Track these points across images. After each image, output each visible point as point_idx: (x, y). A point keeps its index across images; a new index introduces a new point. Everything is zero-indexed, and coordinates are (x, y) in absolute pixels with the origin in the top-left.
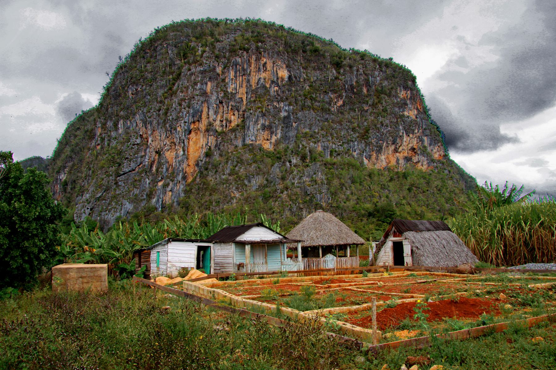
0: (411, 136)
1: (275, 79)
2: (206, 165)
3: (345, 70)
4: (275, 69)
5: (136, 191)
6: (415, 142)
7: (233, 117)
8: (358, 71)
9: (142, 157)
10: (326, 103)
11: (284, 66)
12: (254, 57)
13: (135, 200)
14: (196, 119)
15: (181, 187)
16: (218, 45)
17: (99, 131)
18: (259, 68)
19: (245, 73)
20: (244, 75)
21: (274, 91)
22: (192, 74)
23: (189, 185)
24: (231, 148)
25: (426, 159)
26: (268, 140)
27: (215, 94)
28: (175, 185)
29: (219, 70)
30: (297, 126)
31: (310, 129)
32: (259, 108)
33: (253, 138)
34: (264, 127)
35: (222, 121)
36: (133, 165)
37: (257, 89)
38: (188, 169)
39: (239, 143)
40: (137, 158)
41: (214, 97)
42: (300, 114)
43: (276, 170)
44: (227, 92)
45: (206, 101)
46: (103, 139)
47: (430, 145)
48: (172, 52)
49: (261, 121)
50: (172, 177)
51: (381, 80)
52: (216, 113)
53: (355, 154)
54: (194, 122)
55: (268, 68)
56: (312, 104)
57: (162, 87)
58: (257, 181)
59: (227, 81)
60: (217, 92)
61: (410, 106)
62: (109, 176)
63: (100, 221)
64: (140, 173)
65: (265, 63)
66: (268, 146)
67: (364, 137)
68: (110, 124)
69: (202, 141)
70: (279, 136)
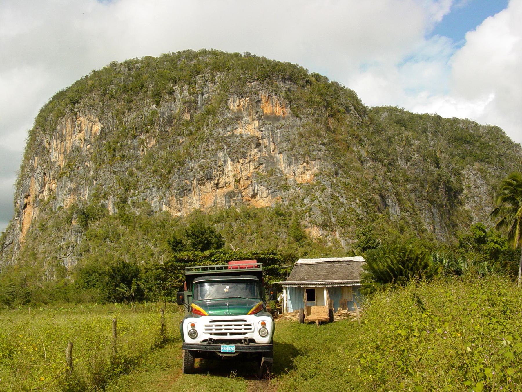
11: (97, 120)
47: (289, 165)
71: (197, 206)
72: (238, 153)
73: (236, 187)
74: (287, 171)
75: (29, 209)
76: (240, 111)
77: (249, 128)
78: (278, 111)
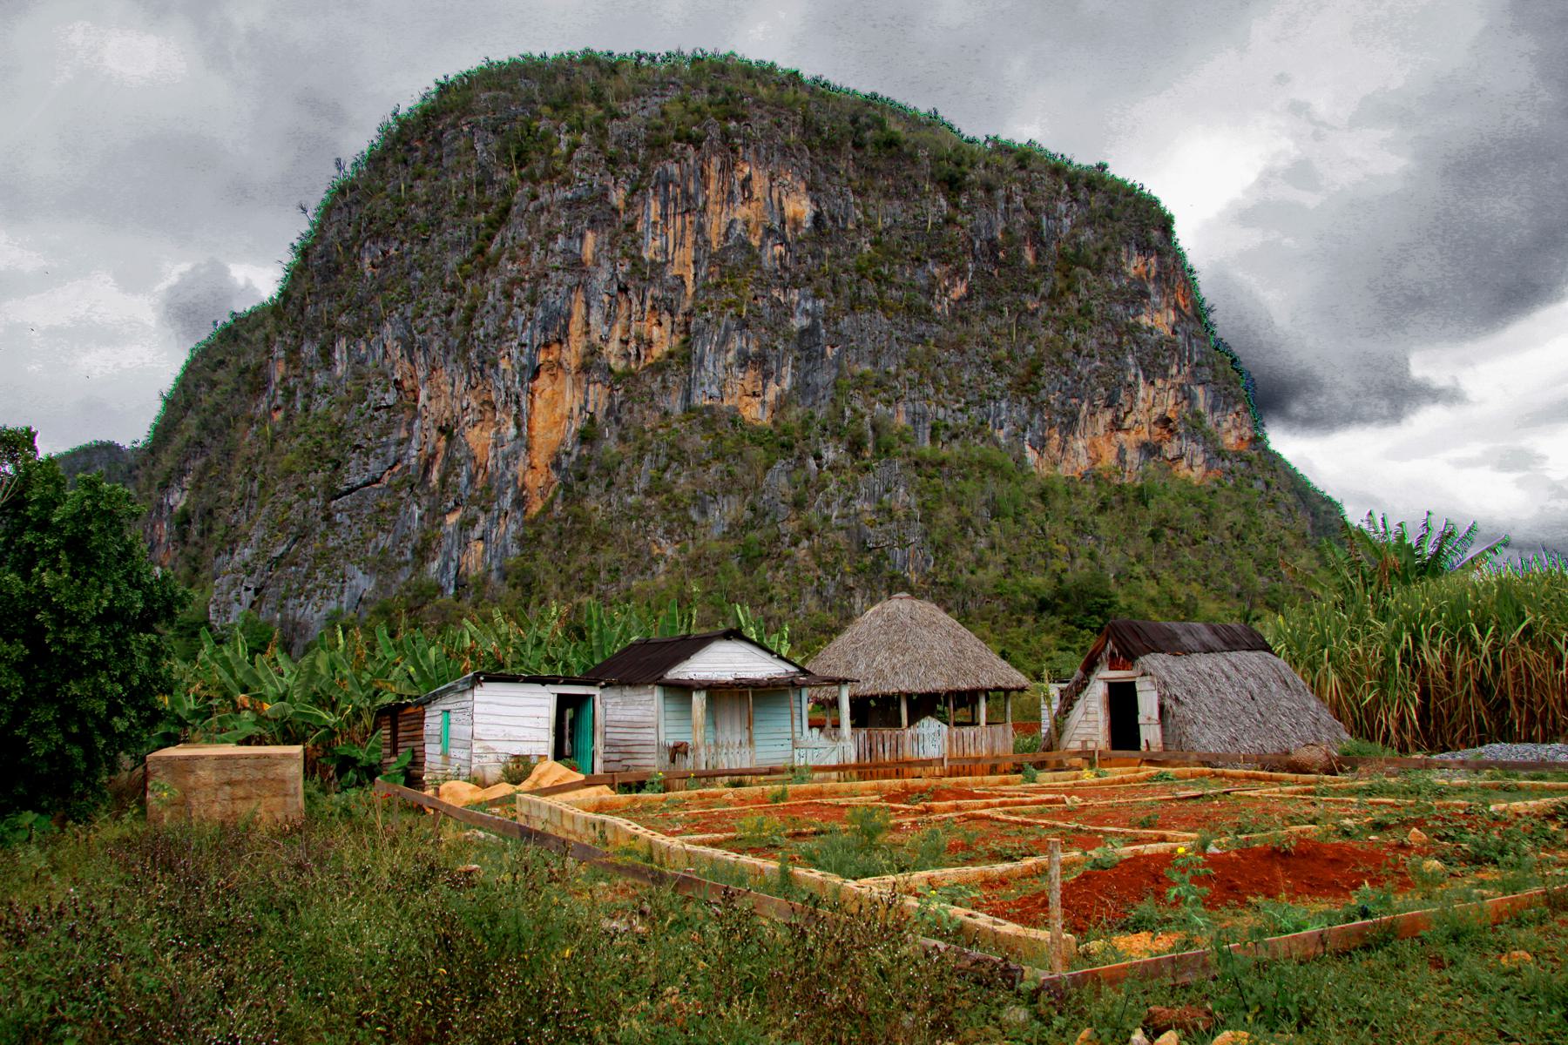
0: (1159, 383)
1: (777, 223)
2: (582, 467)
3: (972, 199)
4: (775, 195)
5: (385, 541)
6: (1171, 402)
7: (656, 331)
8: (1008, 199)
9: (400, 443)
10: (921, 290)
11: (802, 187)
12: (716, 161)
13: (382, 566)
14: (551, 335)
15: (509, 529)
16: (615, 127)
17: (278, 371)
18: (731, 193)
19: (690, 205)
20: (688, 211)
21: (774, 258)
22: (541, 209)
23: (532, 522)
24: (652, 419)
25: (1201, 448)
26: (754, 394)
27: (607, 265)
28: (495, 522)
29: (617, 197)
30: (839, 357)
31: (875, 364)
32: (730, 305)
33: (714, 390)
34: (744, 360)
35: (625, 342)
36: (374, 466)
37: (725, 250)
38: (529, 478)
39: (675, 404)
40: (386, 445)
41: (603, 275)
42: (846, 322)
43: (779, 481)
44: (641, 259)
45: (582, 286)
46: (290, 394)
47: (1213, 409)
48: (484, 148)
49: (737, 342)
50: (486, 499)
51: (1074, 226)
52: (609, 319)
53: (1001, 435)
54: (547, 346)
55: (757, 193)
56: (881, 294)
57: (456, 245)
58: (725, 512)
59: (639, 228)
60: (613, 261)
61: (1157, 300)
62: (307, 497)
63: (283, 624)
64: (394, 489)
65: (749, 179)
66: (755, 413)
67: (1027, 386)
68: (309, 350)
69: (570, 399)
70: (787, 383)
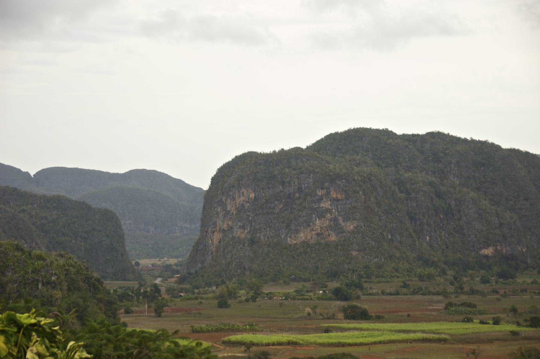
0: (323, 219)
8: (294, 183)
19: (234, 199)
34: (240, 227)
49: (239, 224)
71: (303, 239)
72: (321, 216)
73: (321, 231)
74: (343, 224)
75: (216, 234)
76: (322, 195)
77: (325, 204)
78: (339, 196)
